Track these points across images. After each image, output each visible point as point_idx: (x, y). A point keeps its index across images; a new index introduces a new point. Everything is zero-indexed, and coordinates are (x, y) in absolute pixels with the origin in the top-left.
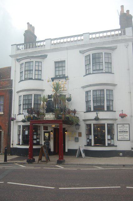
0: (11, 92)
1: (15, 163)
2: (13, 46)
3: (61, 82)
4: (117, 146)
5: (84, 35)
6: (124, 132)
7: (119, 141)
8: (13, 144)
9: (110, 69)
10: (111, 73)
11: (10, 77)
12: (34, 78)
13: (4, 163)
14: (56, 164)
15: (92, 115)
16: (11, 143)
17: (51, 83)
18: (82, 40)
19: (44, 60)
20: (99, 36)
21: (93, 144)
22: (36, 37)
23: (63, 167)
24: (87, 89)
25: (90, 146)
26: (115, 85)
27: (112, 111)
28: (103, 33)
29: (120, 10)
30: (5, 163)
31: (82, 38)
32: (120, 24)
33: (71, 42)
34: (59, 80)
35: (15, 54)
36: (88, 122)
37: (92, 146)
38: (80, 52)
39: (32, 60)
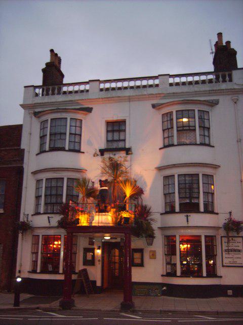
0: (20, 171)
1: (38, 308)
2: (27, 88)
3: (120, 157)
4: (221, 277)
6: (235, 250)
7: (227, 269)
8: (22, 270)
9: (207, 139)
10: (209, 145)
11: (19, 145)
12: (67, 148)
13: (12, 310)
14: (121, 311)
15: (178, 220)
16: (18, 268)
17: (100, 158)
18: (87, 91)
19: (213, 108)
20: (129, 86)
22: (62, 76)
23: (213, 318)
24: (168, 172)
25: (174, 277)
26: (216, 167)
27: (212, 212)
28: (141, 81)
29: (216, 39)
30: (15, 309)
31: (157, 82)
32: (213, 64)
34: (115, 155)
35: (31, 103)
36: (169, 233)
37: (178, 277)
38: (154, 106)
39: (64, 115)
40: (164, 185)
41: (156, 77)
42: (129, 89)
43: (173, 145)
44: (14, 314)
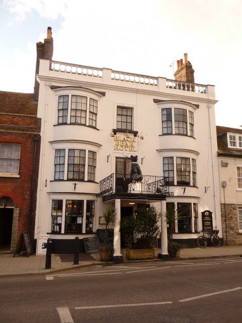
0: (37, 140)
5: (104, 70)
10: (95, 128)
12: (69, 122)
21: (63, 232)
26: (99, 146)
33: (72, 73)
40: (55, 157)
41: (101, 69)
42: (82, 75)
43: (66, 124)
44: (150, 265)
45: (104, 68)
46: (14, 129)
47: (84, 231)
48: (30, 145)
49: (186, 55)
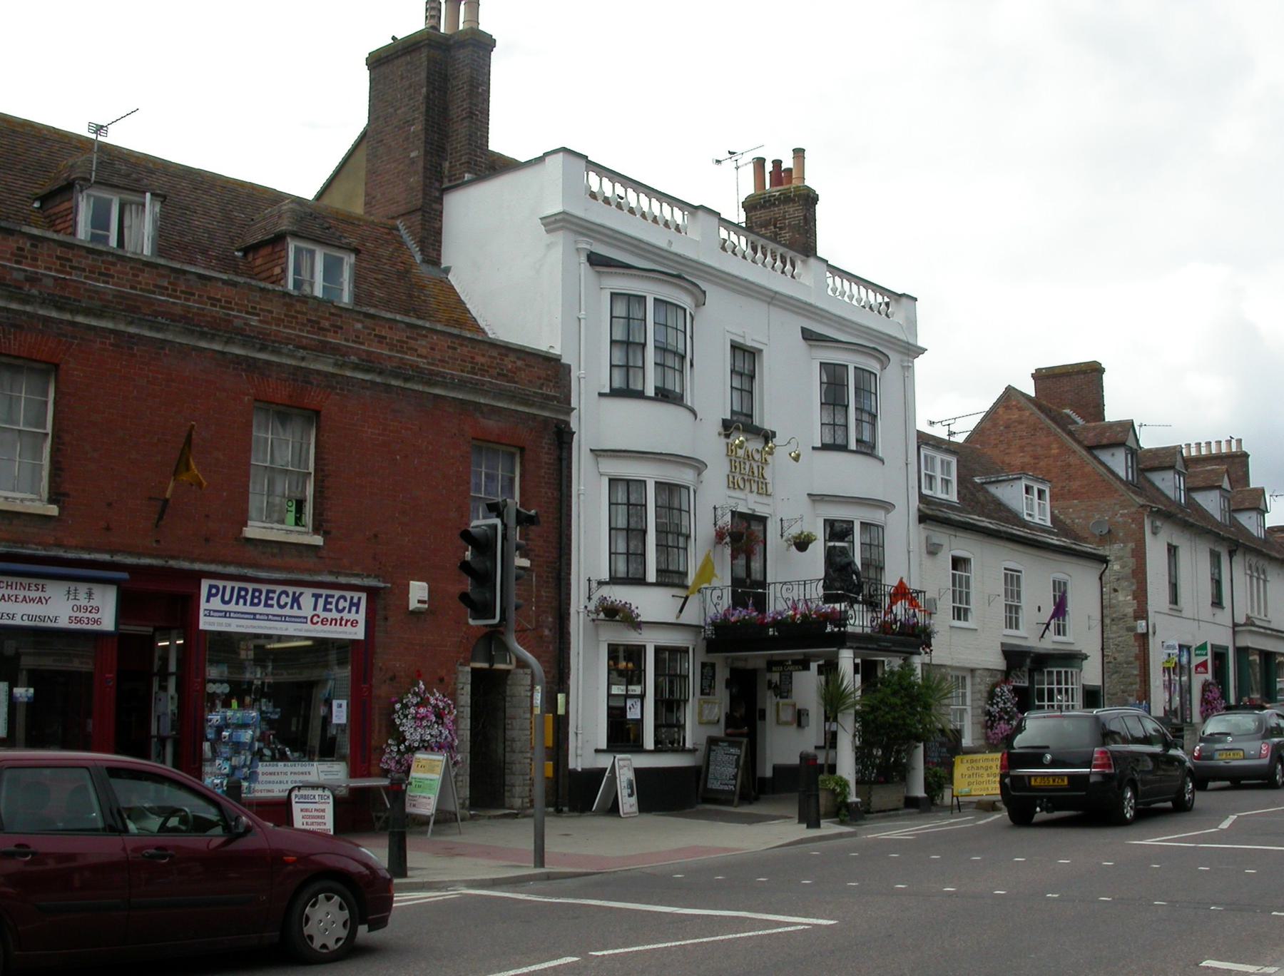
45: (702, 207)
46: (500, 394)
47: (649, 743)
48: (548, 445)
49: (799, 153)
